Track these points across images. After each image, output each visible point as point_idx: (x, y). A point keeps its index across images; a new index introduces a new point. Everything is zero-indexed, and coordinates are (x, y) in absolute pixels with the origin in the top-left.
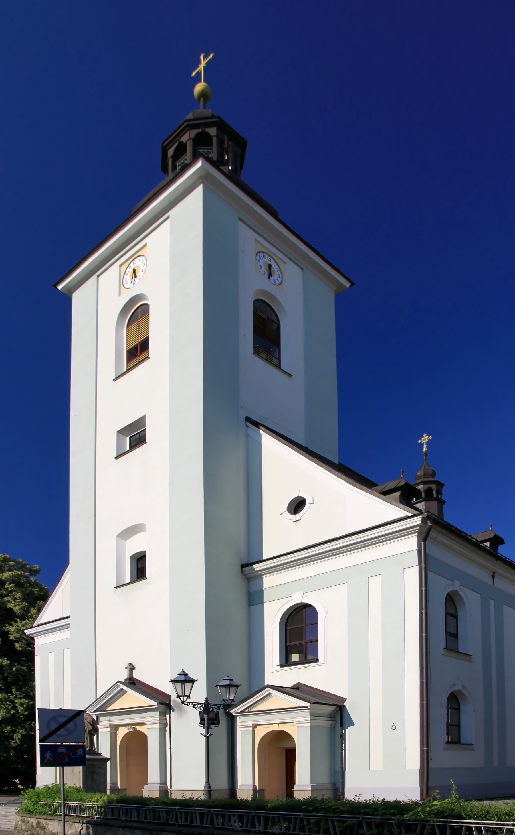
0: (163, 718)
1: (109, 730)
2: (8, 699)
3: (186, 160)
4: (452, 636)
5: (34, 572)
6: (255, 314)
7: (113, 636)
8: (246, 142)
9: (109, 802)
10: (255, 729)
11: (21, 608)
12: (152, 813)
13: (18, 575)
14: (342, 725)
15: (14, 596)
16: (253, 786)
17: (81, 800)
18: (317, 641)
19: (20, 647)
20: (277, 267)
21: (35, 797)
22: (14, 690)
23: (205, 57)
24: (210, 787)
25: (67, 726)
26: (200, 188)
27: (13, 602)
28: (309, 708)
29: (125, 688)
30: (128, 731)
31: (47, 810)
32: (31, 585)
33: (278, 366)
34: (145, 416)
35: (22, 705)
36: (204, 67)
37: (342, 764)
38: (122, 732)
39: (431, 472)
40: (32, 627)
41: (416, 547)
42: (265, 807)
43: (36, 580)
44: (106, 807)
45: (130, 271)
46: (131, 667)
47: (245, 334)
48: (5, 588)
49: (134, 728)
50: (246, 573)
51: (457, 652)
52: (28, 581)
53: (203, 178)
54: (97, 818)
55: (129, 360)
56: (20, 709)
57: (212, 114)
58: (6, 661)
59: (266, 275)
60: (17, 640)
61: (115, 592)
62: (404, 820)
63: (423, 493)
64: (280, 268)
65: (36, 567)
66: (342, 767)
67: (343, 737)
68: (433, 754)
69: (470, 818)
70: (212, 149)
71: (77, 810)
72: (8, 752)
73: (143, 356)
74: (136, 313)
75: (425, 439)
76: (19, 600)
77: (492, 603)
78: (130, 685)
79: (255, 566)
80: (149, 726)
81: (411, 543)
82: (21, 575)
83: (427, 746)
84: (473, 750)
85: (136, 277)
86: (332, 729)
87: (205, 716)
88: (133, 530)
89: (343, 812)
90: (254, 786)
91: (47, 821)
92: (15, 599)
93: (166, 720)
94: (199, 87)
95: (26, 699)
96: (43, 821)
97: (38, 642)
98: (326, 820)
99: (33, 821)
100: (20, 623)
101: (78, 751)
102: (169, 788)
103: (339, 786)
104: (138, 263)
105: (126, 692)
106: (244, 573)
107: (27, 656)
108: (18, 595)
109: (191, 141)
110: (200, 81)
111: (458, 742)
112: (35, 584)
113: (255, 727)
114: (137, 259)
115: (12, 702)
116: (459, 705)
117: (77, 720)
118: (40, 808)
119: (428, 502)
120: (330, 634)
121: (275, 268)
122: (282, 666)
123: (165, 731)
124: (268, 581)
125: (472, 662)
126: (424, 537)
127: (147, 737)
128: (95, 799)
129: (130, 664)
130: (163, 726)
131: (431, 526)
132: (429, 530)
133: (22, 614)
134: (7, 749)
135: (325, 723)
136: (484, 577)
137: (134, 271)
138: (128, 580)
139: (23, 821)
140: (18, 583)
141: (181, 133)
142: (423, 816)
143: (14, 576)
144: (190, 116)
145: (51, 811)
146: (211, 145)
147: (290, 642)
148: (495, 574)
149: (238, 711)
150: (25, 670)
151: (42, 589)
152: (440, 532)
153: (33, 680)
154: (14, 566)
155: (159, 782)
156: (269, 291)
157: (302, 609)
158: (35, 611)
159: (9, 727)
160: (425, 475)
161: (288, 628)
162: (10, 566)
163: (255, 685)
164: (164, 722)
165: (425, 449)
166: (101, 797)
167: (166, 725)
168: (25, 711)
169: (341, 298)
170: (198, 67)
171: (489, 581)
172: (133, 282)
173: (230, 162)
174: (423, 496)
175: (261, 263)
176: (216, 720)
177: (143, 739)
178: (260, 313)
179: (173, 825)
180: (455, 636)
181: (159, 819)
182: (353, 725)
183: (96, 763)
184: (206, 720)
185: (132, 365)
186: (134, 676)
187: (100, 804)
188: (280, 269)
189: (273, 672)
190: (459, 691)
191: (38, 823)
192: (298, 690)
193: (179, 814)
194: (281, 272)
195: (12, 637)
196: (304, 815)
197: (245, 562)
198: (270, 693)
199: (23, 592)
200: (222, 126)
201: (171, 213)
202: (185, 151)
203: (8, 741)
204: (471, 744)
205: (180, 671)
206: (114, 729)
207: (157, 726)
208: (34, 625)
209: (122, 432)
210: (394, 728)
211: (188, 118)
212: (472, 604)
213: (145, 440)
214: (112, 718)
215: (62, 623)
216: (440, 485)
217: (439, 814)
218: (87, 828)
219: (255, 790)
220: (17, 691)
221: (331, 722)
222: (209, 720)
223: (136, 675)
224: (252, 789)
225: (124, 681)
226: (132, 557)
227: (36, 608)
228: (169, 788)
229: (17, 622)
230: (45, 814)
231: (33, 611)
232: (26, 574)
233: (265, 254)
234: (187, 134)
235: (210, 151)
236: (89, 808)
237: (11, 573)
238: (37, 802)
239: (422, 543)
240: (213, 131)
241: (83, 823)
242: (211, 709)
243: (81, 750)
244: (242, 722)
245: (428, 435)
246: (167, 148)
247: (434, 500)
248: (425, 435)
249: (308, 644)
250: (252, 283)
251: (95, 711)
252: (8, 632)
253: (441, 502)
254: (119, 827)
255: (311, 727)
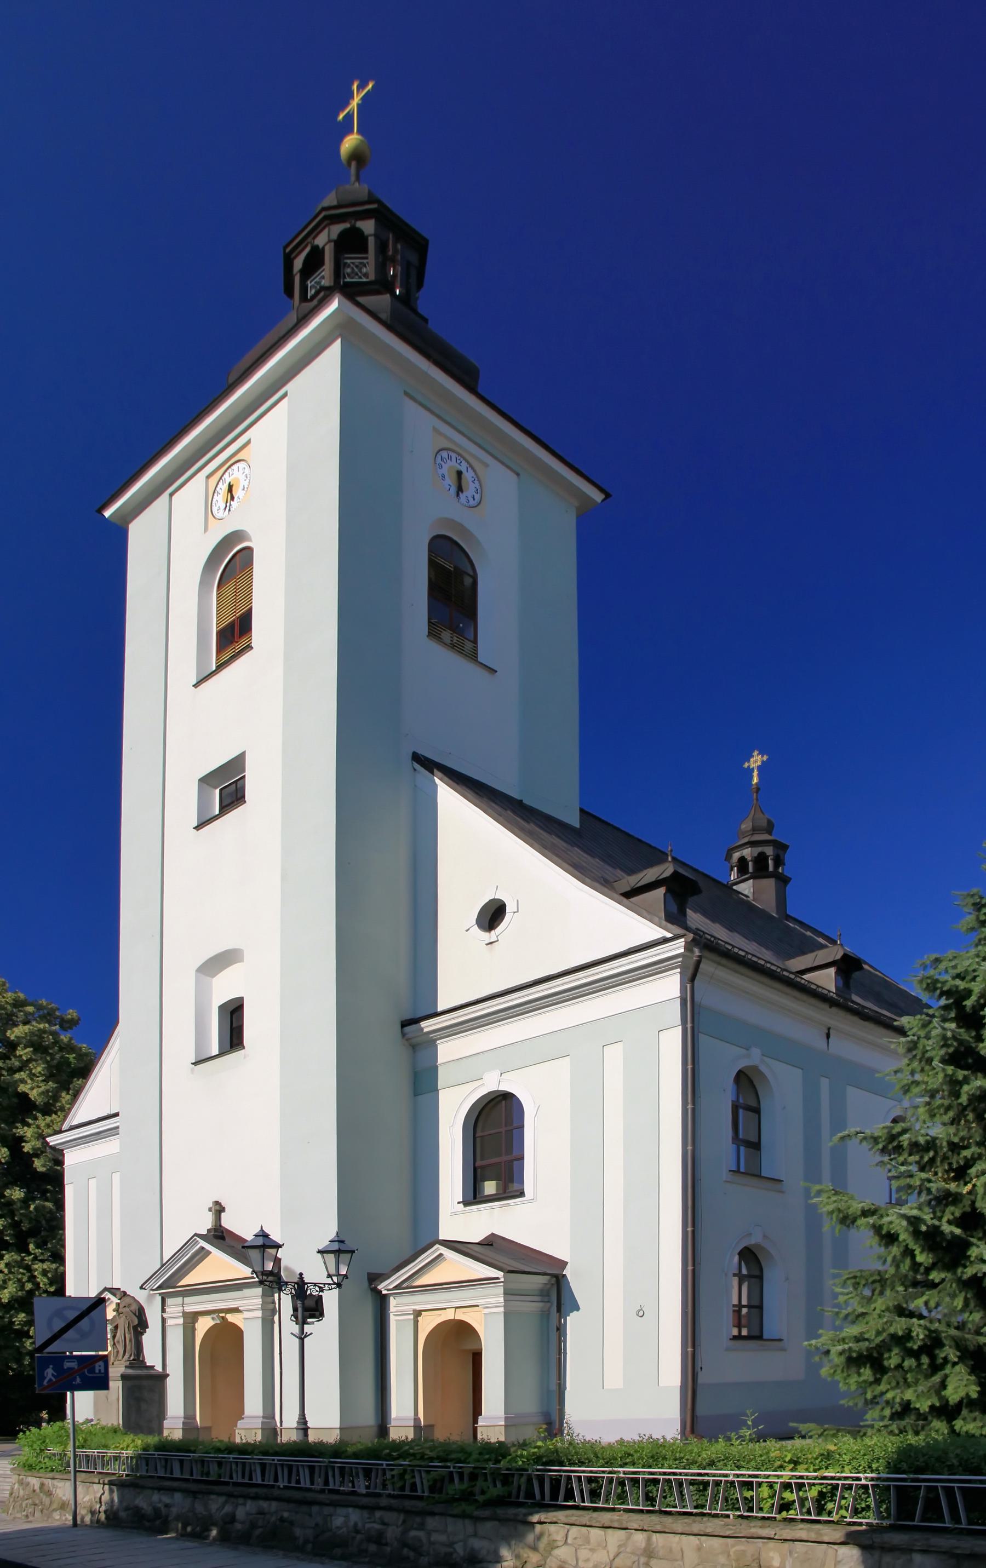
0: (270, 1299)
1: (181, 1321)
2: (20, 1264)
3: (323, 277)
4: (750, 1145)
5: (67, 1024)
6: (432, 564)
7: (190, 1154)
8: (427, 241)
9: (144, 1449)
10: (419, 1318)
11: (43, 1093)
12: (199, 1466)
13: (39, 1030)
14: (559, 1310)
15: (31, 1070)
16: (415, 1419)
17: (106, 1447)
18: (523, 1158)
19: (43, 1166)
20: (473, 474)
21: (39, 1443)
22: (31, 1246)
23: (360, 88)
24: (306, 1423)
25: (63, 1325)
26: (336, 346)
27: (29, 1081)
28: (502, 1280)
29: (208, 1247)
30: (212, 1323)
31: (55, 1463)
32: (61, 1049)
33: (473, 656)
34: (244, 753)
35: (44, 1273)
36: (358, 105)
37: (560, 1379)
38: (203, 1325)
39: (764, 824)
40: (60, 1132)
41: (677, 993)
42: (343, 1452)
43: (71, 1039)
44: (139, 1457)
45: (223, 487)
46: (218, 1207)
47: (417, 594)
48: (15, 1056)
49: (223, 1318)
50: (408, 1036)
51: (759, 1176)
52: (56, 1042)
53: (341, 329)
54: (127, 1475)
55: (219, 650)
56: (42, 1281)
57: (370, 193)
58: (17, 1192)
59: (454, 490)
60: (37, 1154)
61: (192, 1070)
62: (500, 1468)
63: (750, 864)
64: (477, 477)
65: (72, 1013)
66: (560, 1384)
67: (561, 1330)
68: (705, 1358)
69: (571, 1465)
70: (367, 258)
71: (99, 1462)
72: (19, 1361)
73: (243, 643)
74: (232, 564)
75: (756, 760)
76: (40, 1079)
77: (825, 1082)
78: (215, 1241)
79: (423, 1024)
80: (246, 1315)
81: (669, 986)
82: (44, 1031)
83: (694, 1346)
84: (783, 1350)
85: (232, 498)
86: (545, 1315)
87: (299, 1304)
88: (222, 961)
89: (431, 1459)
90: (417, 1419)
91: (55, 1482)
92: (32, 1076)
93: (274, 1302)
94: (350, 143)
95: (53, 1262)
96: (49, 1482)
97: (71, 1158)
98: (413, 1471)
99: (34, 1482)
100: (42, 1121)
101: (97, 1365)
102: (279, 1425)
103: (555, 1417)
104: (237, 474)
105: (209, 1253)
106: (407, 1036)
107: (51, 1183)
108: (39, 1069)
109: (332, 244)
110: (351, 131)
111: (760, 1337)
112: (70, 1048)
113: (418, 1314)
114: (235, 467)
115: (28, 1268)
116: (761, 1270)
117: (94, 1314)
118: (46, 1460)
119: (758, 881)
120: (544, 1147)
121: (468, 476)
122: (466, 1203)
123: (273, 1322)
124: (447, 1050)
125: (783, 1192)
126: (691, 977)
127: (242, 1332)
128: (125, 1444)
129: (217, 1203)
130: (269, 1313)
131: (700, 956)
132: (698, 963)
133: (47, 1104)
134: (19, 1357)
135: (531, 1307)
136: (812, 1037)
137: (230, 488)
138: (215, 1051)
139: (21, 1483)
140: (39, 1047)
141: (316, 231)
142: (520, 1463)
143: (32, 1033)
144: (330, 199)
145: (62, 1465)
146: (365, 250)
147: (482, 1159)
148: (831, 1031)
149: (391, 1287)
150: (51, 1210)
151: (81, 1056)
152: (719, 964)
153: (63, 1228)
154: (32, 1014)
155: (261, 1414)
156: (458, 519)
157: (500, 1102)
158: (68, 1097)
159: (23, 1315)
160: (755, 830)
161: (479, 1134)
162: (27, 1014)
163: (422, 1236)
164: (271, 1306)
165: (755, 780)
166: (133, 1441)
167: (273, 1312)
168: (51, 1284)
169: (588, 522)
170: (347, 104)
171: (820, 1043)
172: (228, 507)
173: (398, 283)
174: (751, 870)
175: (445, 470)
176: (317, 1310)
177: (236, 1334)
178: (441, 561)
179: (227, 1483)
180: (756, 1146)
181: (208, 1474)
182: (578, 1308)
183: (145, 1383)
184: (300, 1310)
185: (225, 657)
186: (223, 1224)
187: (130, 1452)
188: (477, 478)
189: (453, 1214)
190: (758, 1246)
191: (42, 1485)
192: (491, 1249)
193: (234, 1466)
194: (481, 485)
195: (27, 1148)
196: (387, 1465)
197: (408, 1016)
198: (441, 1255)
199: (47, 1062)
200: (383, 216)
201: (289, 387)
202: (321, 263)
203: (20, 1341)
204: (780, 1340)
205: (257, 1230)
206: (191, 1319)
207: (259, 1314)
208: (64, 1128)
209: (206, 781)
210: (641, 1313)
211: (326, 203)
212: (784, 1088)
213: (244, 797)
214: (187, 1300)
215: (106, 1126)
216: (781, 847)
217: (538, 1459)
218: (111, 1491)
219: (417, 1427)
220: (37, 1248)
221: (541, 1304)
222: (305, 1309)
223: (228, 1222)
224: (412, 1423)
225: (205, 1232)
226: (222, 1008)
227: (71, 1092)
228: (279, 1425)
229: (36, 1118)
230: (52, 1470)
231: (65, 1097)
232: (54, 1028)
233: (451, 453)
234: (326, 231)
235: (365, 261)
236: (116, 1458)
237: (27, 1028)
238: (42, 1450)
239: (688, 986)
240: (368, 227)
241: (104, 1484)
242: (309, 1292)
243: (101, 1363)
244: (397, 1305)
245: (762, 753)
246: (293, 256)
247: (769, 876)
248: (756, 753)
249: (515, 1162)
250: (428, 508)
251: (159, 1288)
252: (21, 1139)
253: (783, 881)
254: (153, 1488)
255: (505, 1313)
